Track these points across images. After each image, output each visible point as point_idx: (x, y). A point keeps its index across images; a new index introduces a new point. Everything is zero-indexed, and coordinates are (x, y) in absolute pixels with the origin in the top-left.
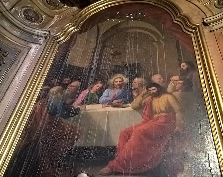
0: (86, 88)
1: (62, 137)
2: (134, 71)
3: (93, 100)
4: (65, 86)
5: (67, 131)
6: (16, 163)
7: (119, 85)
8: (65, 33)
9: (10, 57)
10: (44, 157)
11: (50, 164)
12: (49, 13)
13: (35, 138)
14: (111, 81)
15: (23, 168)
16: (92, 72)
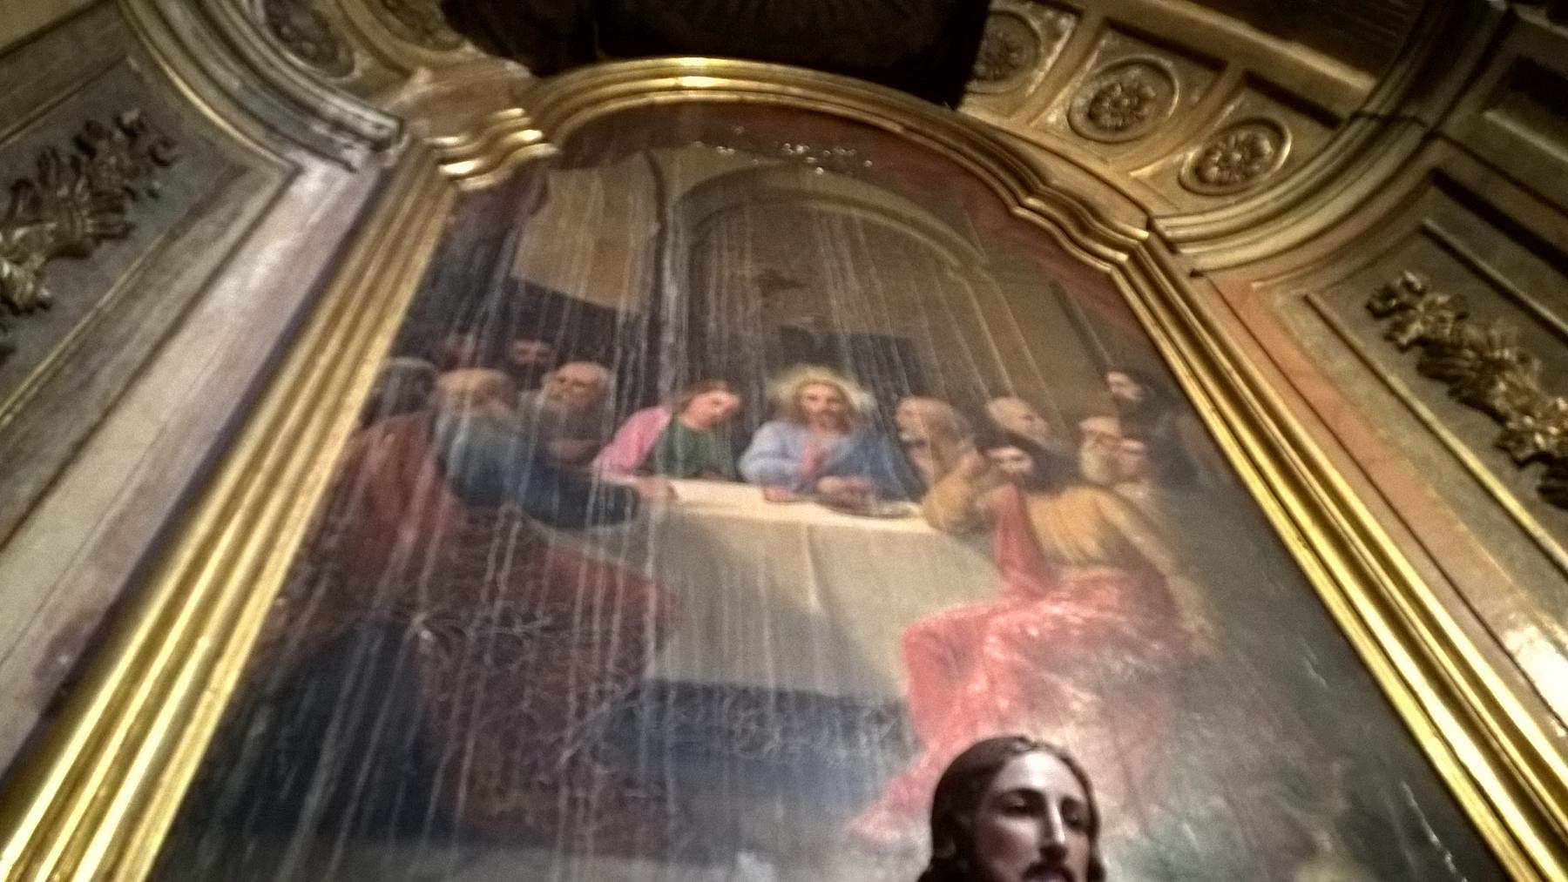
0: (651, 400)
1: (561, 623)
2: (891, 366)
3: (717, 454)
4: (527, 377)
5: (590, 593)
6: (270, 737)
7: (827, 412)
8: (493, 148)
9: (181, 180)
10: (465, 719)
11: (508, 765)
12: (387, 49)
13: (381, 603)
14: (784, 389)
15: (321, 777)
16: (668, 338)
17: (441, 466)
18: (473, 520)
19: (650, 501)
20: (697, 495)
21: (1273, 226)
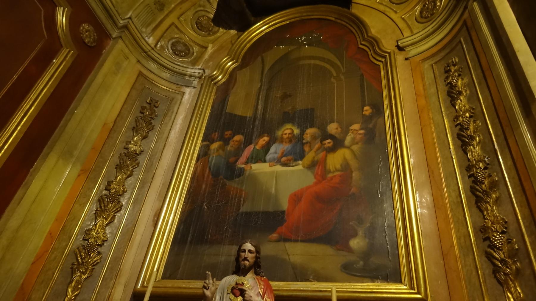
0: (250, 144)
3: (259, 157)
4: (226, 141)
16: (257, 123)
17: (210, 169)
18: (214, 181)
19: (246, 170)
20: (257, 167)
21: (432, 37)
